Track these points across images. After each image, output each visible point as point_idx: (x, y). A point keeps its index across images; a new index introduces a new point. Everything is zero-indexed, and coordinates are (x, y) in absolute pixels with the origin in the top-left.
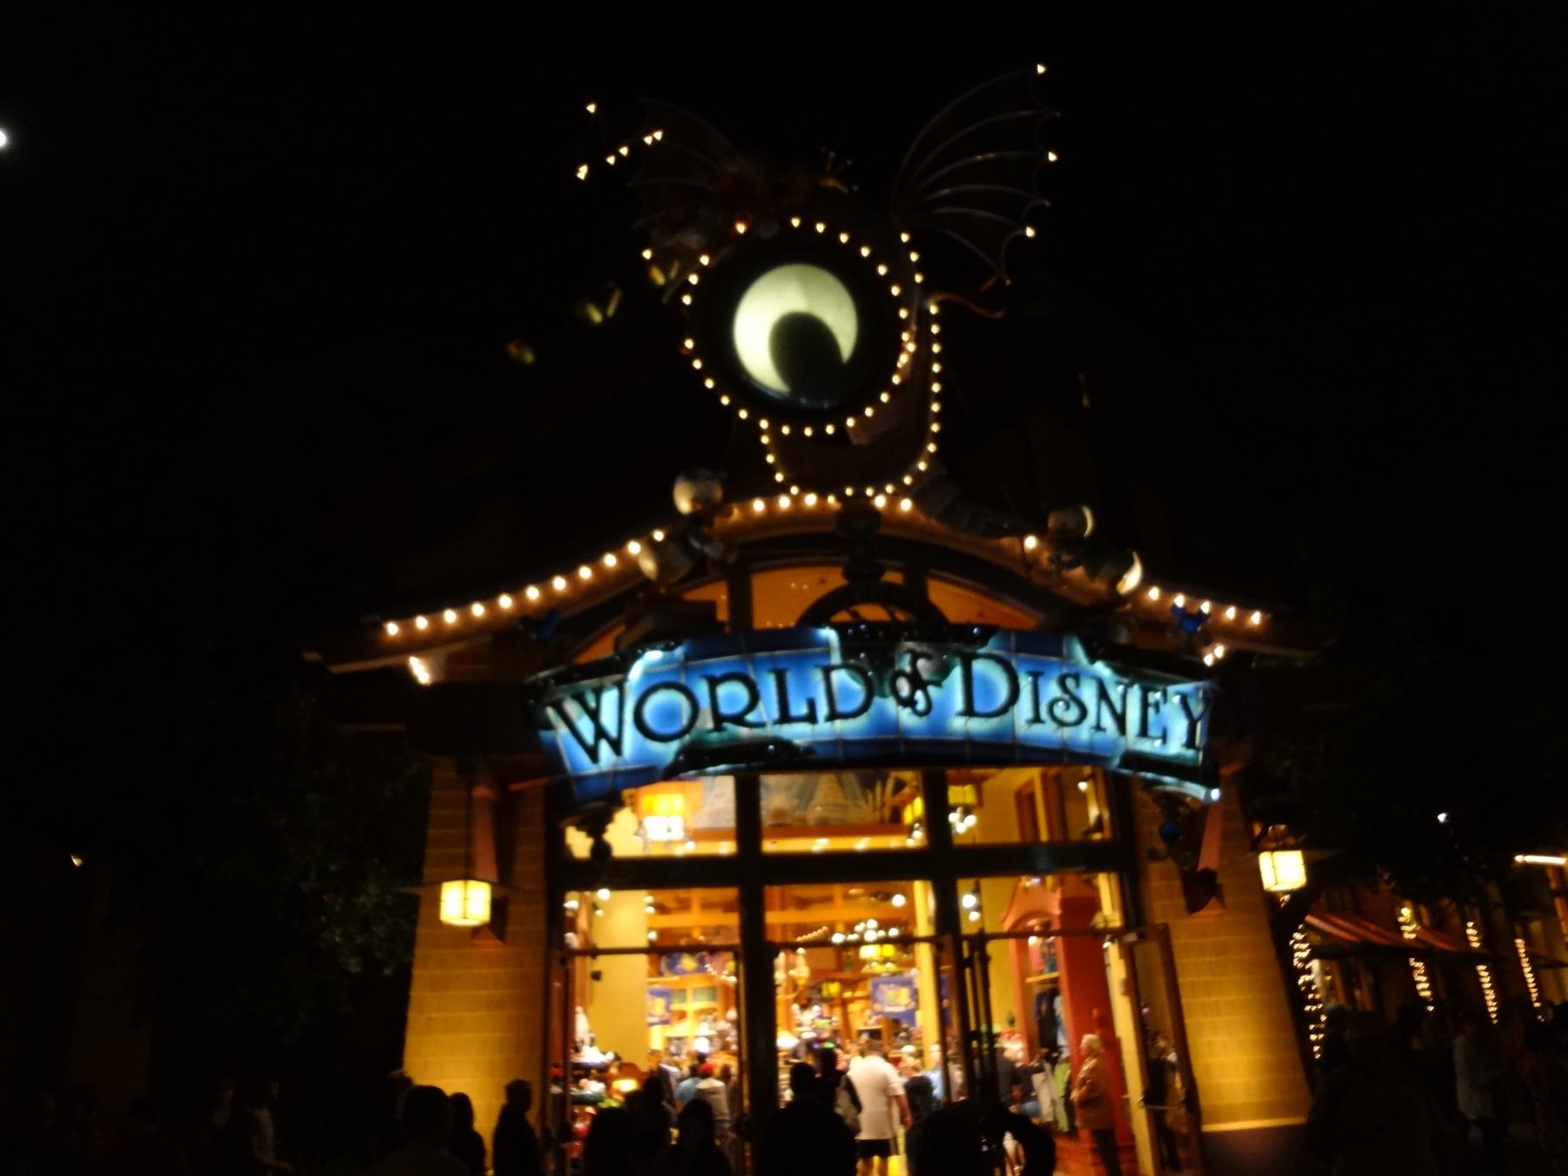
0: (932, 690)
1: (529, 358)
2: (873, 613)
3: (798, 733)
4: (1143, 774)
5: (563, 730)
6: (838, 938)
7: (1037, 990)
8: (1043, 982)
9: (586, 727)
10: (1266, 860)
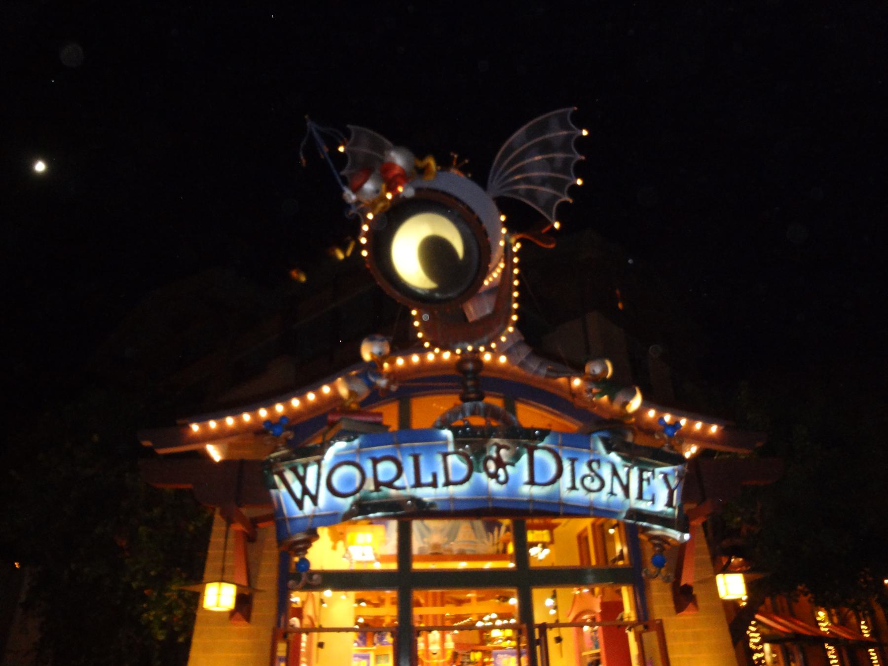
0: (509, 468)
1: (303, 279)
2: (478, 421)
3: (426, 494)
4: (640, 523)
5: (283, 490)
6: (479, 624)
7: (589, 660)
8: (592, 655)
9: (297, 488)
10: (721, 579)
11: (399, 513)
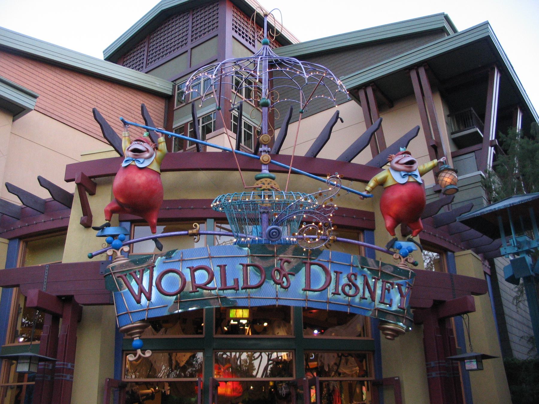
11: (190, 232)
